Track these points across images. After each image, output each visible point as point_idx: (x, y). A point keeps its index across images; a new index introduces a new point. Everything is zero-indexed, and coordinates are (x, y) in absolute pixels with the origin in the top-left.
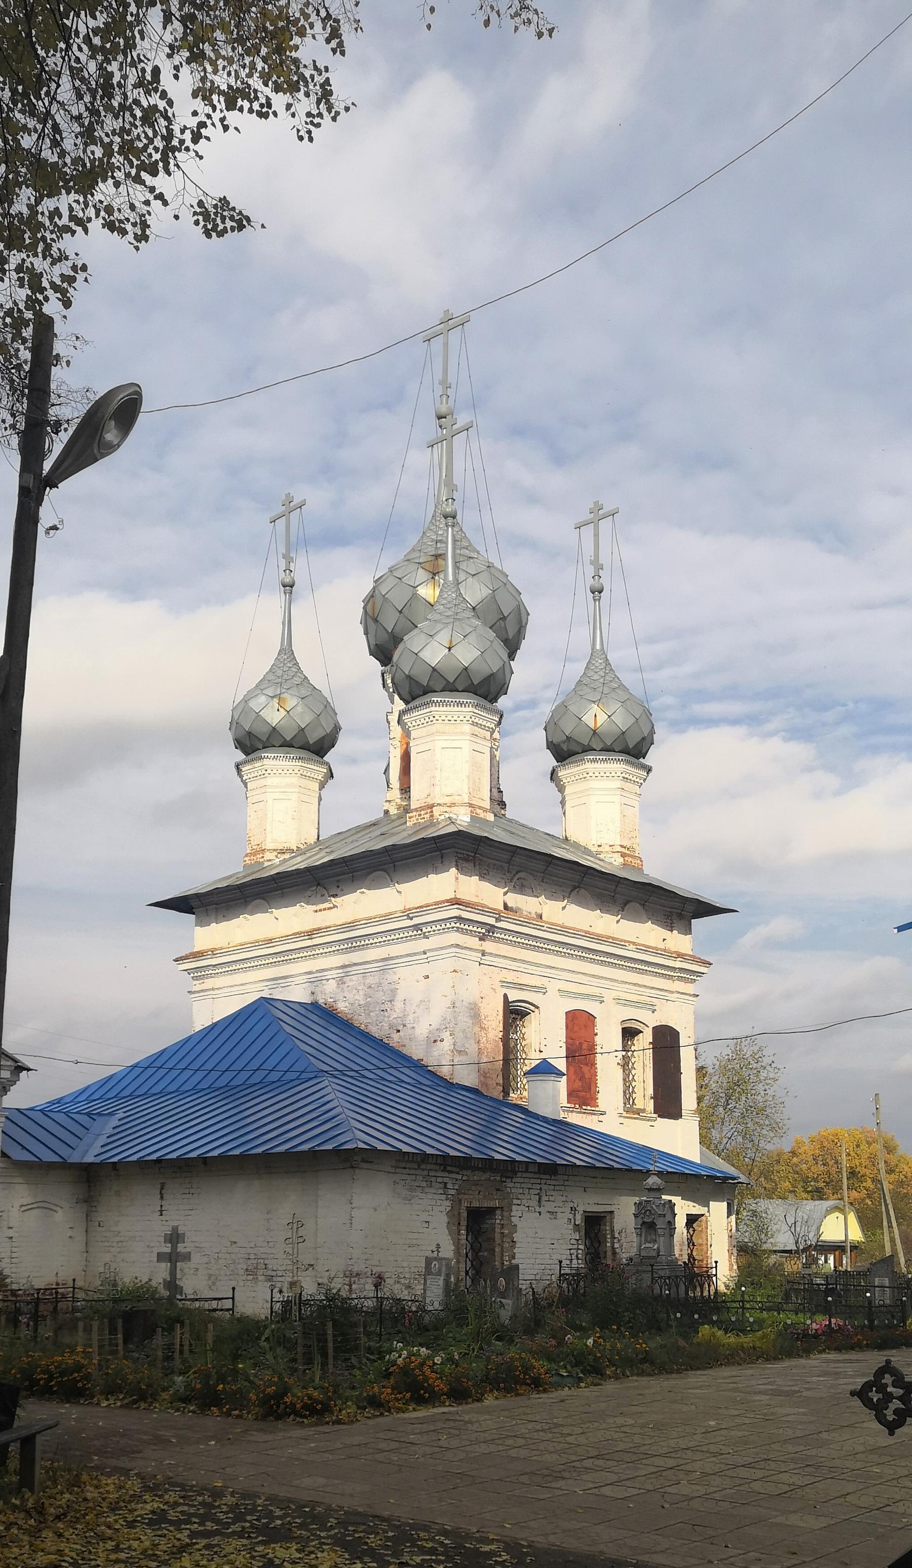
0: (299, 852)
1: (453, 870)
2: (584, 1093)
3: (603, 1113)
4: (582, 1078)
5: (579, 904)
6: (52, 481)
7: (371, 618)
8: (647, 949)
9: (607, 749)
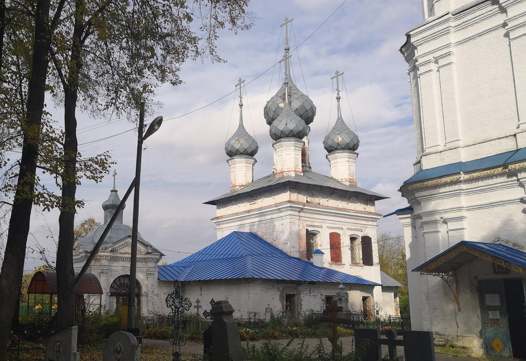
0: (246, 186)
1: (289, 192)
2: (336, 258)
3: (344, 265)
4: (336, 253)
5: (333, 199)
6: (145, 138)
7: (266, 114)
8: (358, 212)
9: (343, 149)
